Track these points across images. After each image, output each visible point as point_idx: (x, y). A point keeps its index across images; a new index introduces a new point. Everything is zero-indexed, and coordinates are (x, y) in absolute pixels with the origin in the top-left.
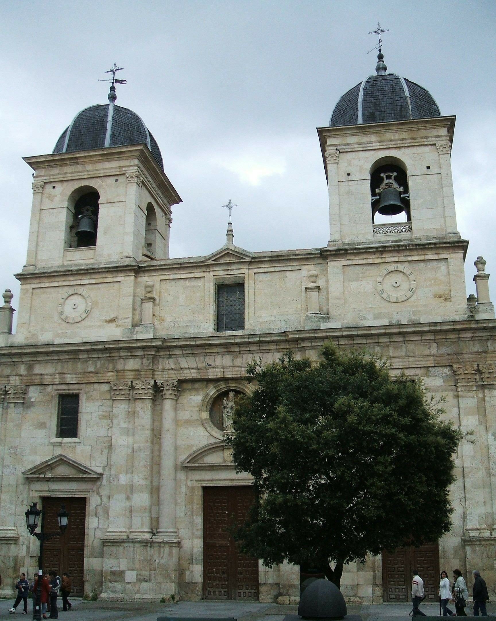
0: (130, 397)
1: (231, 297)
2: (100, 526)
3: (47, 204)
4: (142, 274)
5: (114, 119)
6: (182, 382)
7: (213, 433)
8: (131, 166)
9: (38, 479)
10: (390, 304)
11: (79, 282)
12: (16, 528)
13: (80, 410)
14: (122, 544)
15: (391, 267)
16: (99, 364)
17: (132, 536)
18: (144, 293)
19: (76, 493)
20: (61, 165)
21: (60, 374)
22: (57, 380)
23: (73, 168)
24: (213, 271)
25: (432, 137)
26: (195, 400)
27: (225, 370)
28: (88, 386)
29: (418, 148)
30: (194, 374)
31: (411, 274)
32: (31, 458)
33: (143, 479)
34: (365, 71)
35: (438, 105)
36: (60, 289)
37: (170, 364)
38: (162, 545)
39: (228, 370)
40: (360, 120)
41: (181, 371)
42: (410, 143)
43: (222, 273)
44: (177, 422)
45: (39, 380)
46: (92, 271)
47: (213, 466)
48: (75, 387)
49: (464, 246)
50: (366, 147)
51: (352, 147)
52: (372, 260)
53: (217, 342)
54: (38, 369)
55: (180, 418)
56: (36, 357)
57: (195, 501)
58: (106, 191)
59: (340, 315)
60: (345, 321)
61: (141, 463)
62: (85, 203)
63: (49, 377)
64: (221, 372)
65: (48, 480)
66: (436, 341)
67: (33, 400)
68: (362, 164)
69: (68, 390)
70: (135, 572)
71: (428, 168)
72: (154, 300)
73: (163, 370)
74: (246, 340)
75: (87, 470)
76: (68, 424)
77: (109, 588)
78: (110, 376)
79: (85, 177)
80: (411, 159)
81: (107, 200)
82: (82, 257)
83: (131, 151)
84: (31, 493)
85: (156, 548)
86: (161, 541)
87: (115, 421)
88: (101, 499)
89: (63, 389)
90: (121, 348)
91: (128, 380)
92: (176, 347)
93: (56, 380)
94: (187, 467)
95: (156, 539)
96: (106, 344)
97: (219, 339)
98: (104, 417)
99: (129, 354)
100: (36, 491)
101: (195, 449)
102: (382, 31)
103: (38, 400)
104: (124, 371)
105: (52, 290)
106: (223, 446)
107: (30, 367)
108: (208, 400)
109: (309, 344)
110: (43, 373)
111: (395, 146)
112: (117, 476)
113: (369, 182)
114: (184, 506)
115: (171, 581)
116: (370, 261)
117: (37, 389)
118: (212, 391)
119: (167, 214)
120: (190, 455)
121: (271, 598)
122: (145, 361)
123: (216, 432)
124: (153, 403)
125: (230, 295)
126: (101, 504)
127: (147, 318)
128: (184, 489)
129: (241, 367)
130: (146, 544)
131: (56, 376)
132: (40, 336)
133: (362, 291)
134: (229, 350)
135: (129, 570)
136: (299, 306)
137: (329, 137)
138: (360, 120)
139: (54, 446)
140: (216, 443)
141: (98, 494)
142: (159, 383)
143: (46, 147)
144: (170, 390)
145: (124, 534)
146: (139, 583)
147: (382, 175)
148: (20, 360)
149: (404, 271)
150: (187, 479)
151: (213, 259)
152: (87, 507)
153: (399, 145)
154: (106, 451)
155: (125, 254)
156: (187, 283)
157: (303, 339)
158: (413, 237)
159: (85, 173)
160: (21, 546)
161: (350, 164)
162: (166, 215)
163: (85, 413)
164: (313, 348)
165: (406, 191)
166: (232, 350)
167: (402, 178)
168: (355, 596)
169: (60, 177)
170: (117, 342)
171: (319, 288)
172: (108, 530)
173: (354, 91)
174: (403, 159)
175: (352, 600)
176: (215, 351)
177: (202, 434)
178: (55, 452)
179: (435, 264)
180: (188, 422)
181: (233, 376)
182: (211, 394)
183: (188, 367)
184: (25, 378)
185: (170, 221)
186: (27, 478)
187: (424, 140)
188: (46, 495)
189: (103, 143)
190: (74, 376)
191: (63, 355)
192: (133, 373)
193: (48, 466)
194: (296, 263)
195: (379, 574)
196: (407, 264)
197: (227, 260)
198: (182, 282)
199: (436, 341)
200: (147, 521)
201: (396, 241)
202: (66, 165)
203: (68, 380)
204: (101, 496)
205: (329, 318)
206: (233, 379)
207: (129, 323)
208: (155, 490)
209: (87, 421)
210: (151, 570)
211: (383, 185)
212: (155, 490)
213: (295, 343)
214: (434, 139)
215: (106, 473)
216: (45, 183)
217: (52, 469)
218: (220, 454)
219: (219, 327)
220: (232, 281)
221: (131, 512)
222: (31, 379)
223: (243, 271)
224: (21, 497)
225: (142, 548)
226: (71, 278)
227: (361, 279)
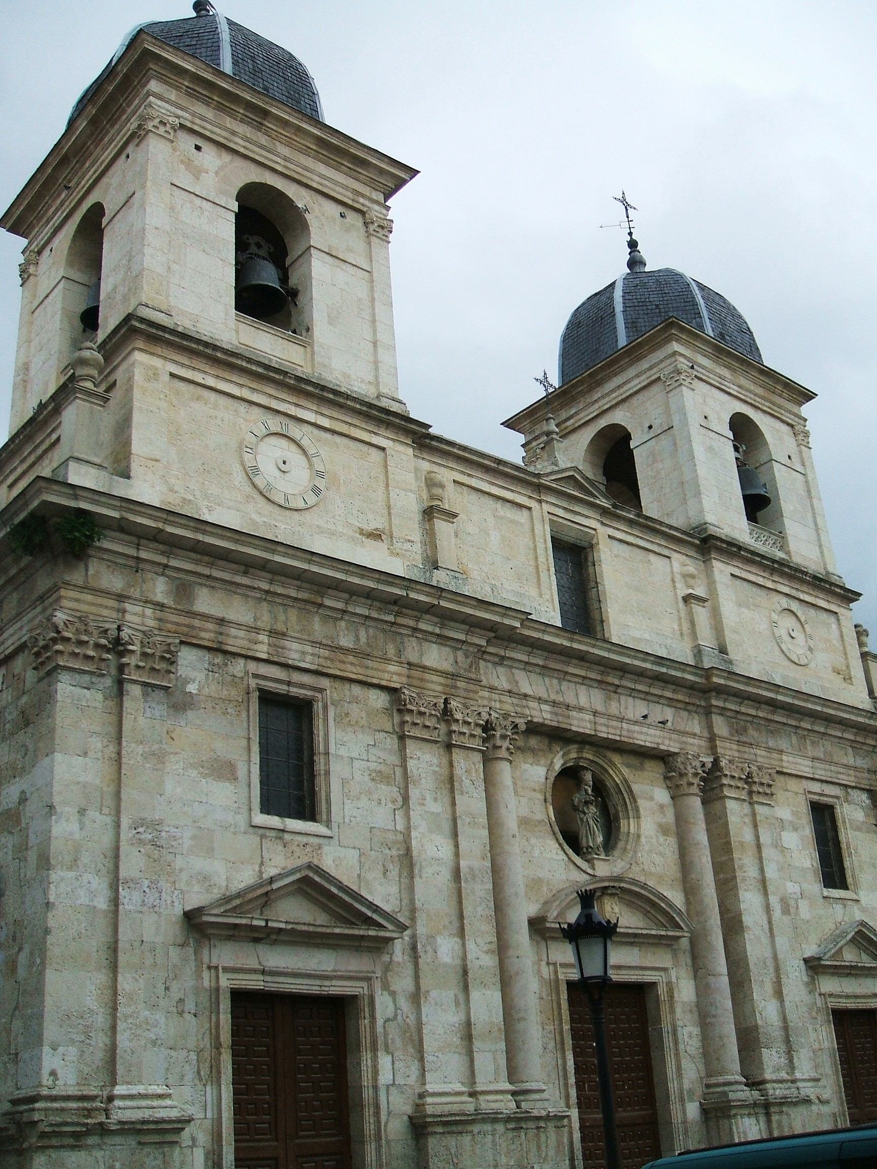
10: (790, 664)
14: (469, 1128)
19: (334, 983)
20: (220, 108)
21: (273, 633)
28: (338, 684)
33: (487, 953)
37: (499, 677)
43: (560, 512)
46: (331, 396)
48: (306, 679)
54: (206, 602)
56: (211, 565)
61: (479, 909)
63: (241, 634)
66: (854, 745)
67: (192, 688)
93: (259, 647)
96: (413, 589)
105: (223, 401)
107: (183, 591)
112: (431, 938)
117: (201, 659)
137: (677, 341)
139: (262, 837)
151: (554, 477)
154: (394, 871)
159: (279, 160)
169: (219, 135)
173: (612, 285)
177: (555, 857)
190: (309, 649)
191: (283, 584)
192: (442, 680)
193: (264, 895)
199: (854, 745)
202: (232, 114)
203: (295, 656)
209: (344, 782)
214: (796, 419)
222: (192, 627)
225: (510, 1135)
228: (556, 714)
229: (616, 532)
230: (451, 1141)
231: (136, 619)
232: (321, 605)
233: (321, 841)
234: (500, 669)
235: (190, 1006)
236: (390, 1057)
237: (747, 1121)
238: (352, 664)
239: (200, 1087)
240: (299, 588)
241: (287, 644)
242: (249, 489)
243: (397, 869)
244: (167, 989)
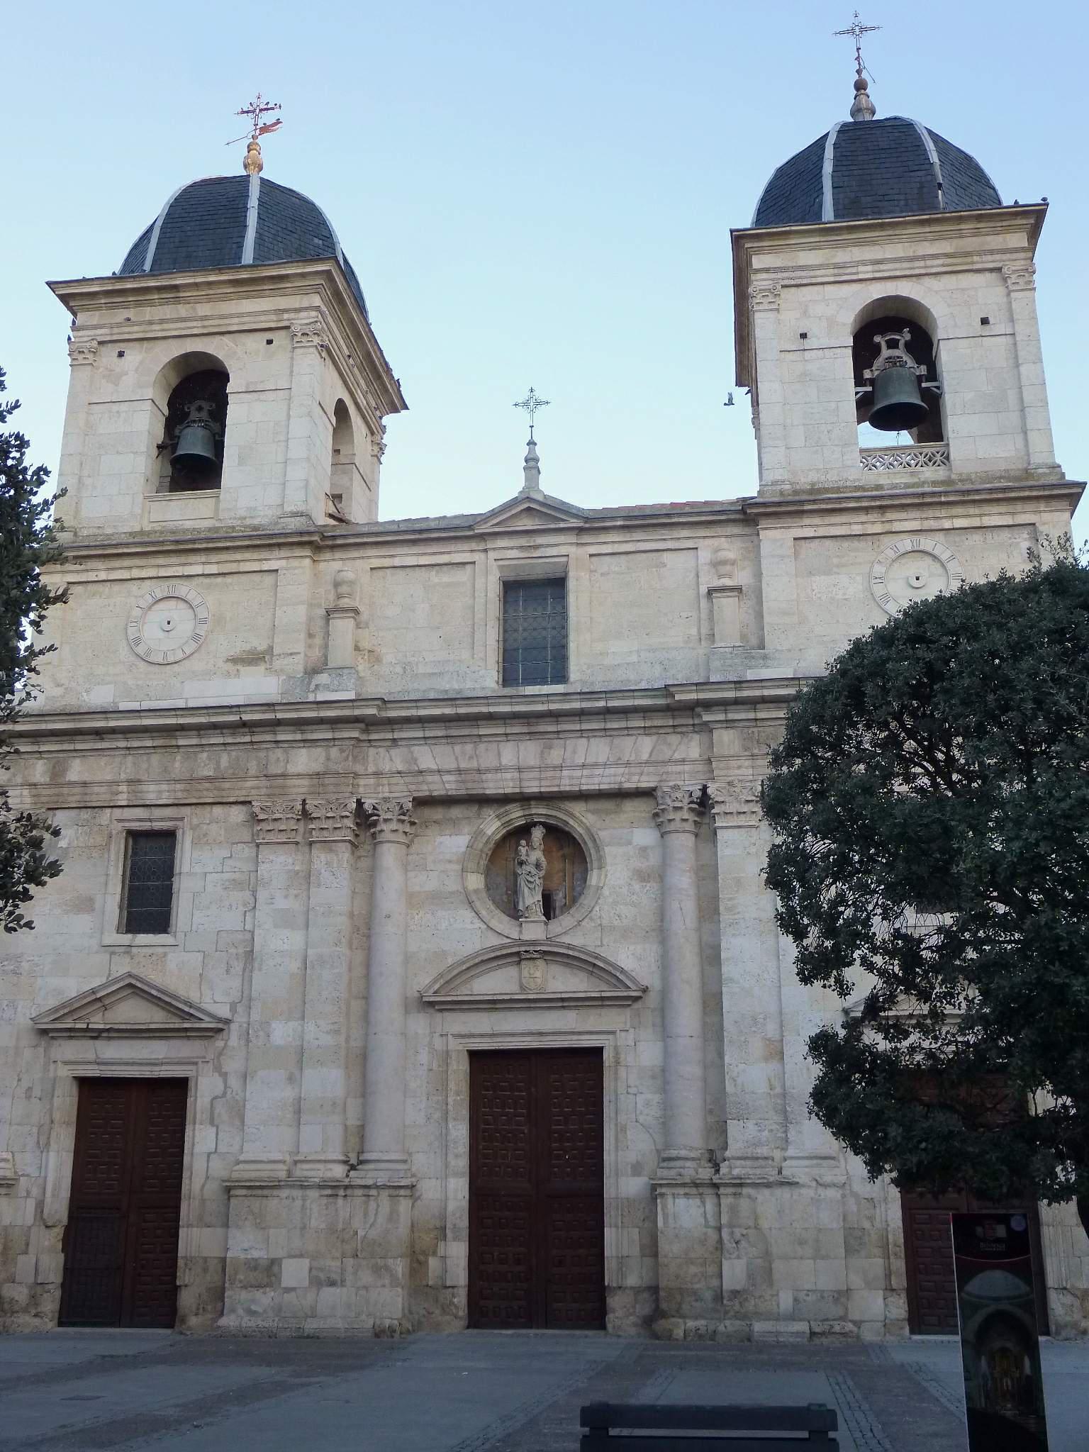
0: (299, 839)
1: (535, 610)
2: (222, 1149)
3: (106, 391)
4: (327, 555)
5: (261, 203)
6: (422, 802)
7: (494, 923)
8: (306, 309)
9: (72, 1034)
11: (179, 571)
12: (9, 1156)
13: (177, 870)
14: (275, 1192)
15: (906, 543)
16: (225, 760)
17: (300, 1171)
18: (332, 597)
19: (163, 1068)
22: (125, 796)
23: (168, 311)
24: (494, 549)
25: (992, 252)
26: (454, 844)
27: (525, 776)
28: (199, 810)
29: (960, 276)
30: (450, 785)
31: (952, 557)
33: (328, 1033)
34: (832, 114)
35: (997, 187)
36: (133, 587)
37: (393, 760)
38: (373, 1192)
39: (532, 775)
40: (828, 212)
41: (421, 779)
42: (943, 265)
44: (413, 900)
47: (494, 1002)
49: (1071, 495)
50: (840, 275)
51: (812, 273)
52: (860, 527)
53: (507, 709)
54: (76, 771)
55: (417, 888)
57: (452, 1085)
58: (245, 365)
59: (789, 650)
60: (802, 664)
62: (198, 392)
63: (103, 789)
64: (512, 779)
65: (96, 1035)
68: (835, 312)
69: (150, 820)
70: (306, 1263)
71: (985, 321)
72: (356, 611)
73: (377, 774)
74: (576, 705)
75: (192, 1011)
78: (249, 788)
79: (196, 331)
80: (946, 303)
81: (248, 385)
82: (190, 511)
83: (303, 275)
84: (52, 1067)
85: (359, 1201)
86: (370, 1182)
87: (262, 895)
88: (225, 1082)
89: (138, 819)
90: (279, 722)
91: (294, 797)
92: (408, 721)
93: (120, 797)
94: (431, 1004)
95: (357, 1178)
96: (245, 712)
97: (511, 704)
98: (236, 885)
99: (299, 737)
100: (66, 1063)
101: (450, 961)
102: (863, 30)
104: (284, 776)
106: (518, 953)
108: (481, 845)
109: (721, 717)
110: (88, 779)
111: (908, 272)
112: (265, 1024)
113: (850, 351)
114: (424, 1098)
115: (395, 1283)
116: (857, 529)
118: (492, 825)
119: (376, 431)
120: (441, 975)
121: (635, 1325)
122: (334, 752)
123: (501, 922)
124: (353, 853)
125: (535, 601)
126: (224, 1094)
127: (342, 651)
128: (424, 1057)
129: (561, 768)
130: (333, 1189)
131: (120, 788)
133: (840, 597)
134: (533, 729)
136: (694, 631)
137: (760, 251)
138: (828, 212)
140: (503, 947)
141: (218, 1068)
142: (367, 807)
143: (106, 260)
144: (395, 821)
145: (281, 1166)
147: (877, 339)
148: (35, 748)
149: (936, 552)
150: (432, 1033)
151: (495, 521)
152: (190, 1101)
153: (917, 272)
154: (238, 967)
155: (289, 508)
156: (434, 577)
157: (708, 705)
158: (953, 477)
161: (805, 313)
162: (372, 433)
163: (190, 874)
164: (729, 724)
165: (933, 374)
166: (541, 728)
167: (923, 346)
168: (843, 1318)
170: (270, 706)
171: (739, 589)
172: (242, 1158)
173: (820, 144)
174: (926, 302)
175: (837, 1329)
176: (500, 730)
178: (114, 968)
179: (1005, 534)
180: (437, 898)
181: (543, 790)
182: (489, 832)
183: (435, 767)
184: (44, 792)
185: (382, 449)
186: (44, 1032)
187: (976, 258)
188: (90, 1074)
189: (239, 257)
190: (164, 787)
193: (97, 1000)
194: (685, 533)
195: (899, 1265)
196: (940, 537)
197: (528, 523)
198: (422, 573)
200: (336, 1133)
201: (913, 485)
202: (151, 303)
203: (152, 796)
204: (226, 1074)
205: (765, 657)
206: (542, 798)
207: (296, 666)
208: (361, 1062)
210: (343, 1256)
211: (878, 363)
212: (361, 1062)
213: (689, 713)
214: (997, 257)
215: (240, 1019)
216: (100, 343)
217: (105, 1008)
218: (512, 971)
219: (508, 678)
220: (538, 573)
221: (298, 1112)
223: (563, 550)
225: (324, 1201)
226: (161, 560)
227: (835, 570)
228: (463, 782)
229: (604, 546)
230: (256, 1204)
231: (18, 801)
232: (178, 747)
233: (167, 949)
234: (394, 752)
235: (37, 1092)
236: (214, 1129)
237: (681, 1202)
238: (207, 790)
239: (38, 1153)
240: (152, 738)
241: (144, 788)
242: (133, 658)
243: (242, 965)
244: (19, 1080)
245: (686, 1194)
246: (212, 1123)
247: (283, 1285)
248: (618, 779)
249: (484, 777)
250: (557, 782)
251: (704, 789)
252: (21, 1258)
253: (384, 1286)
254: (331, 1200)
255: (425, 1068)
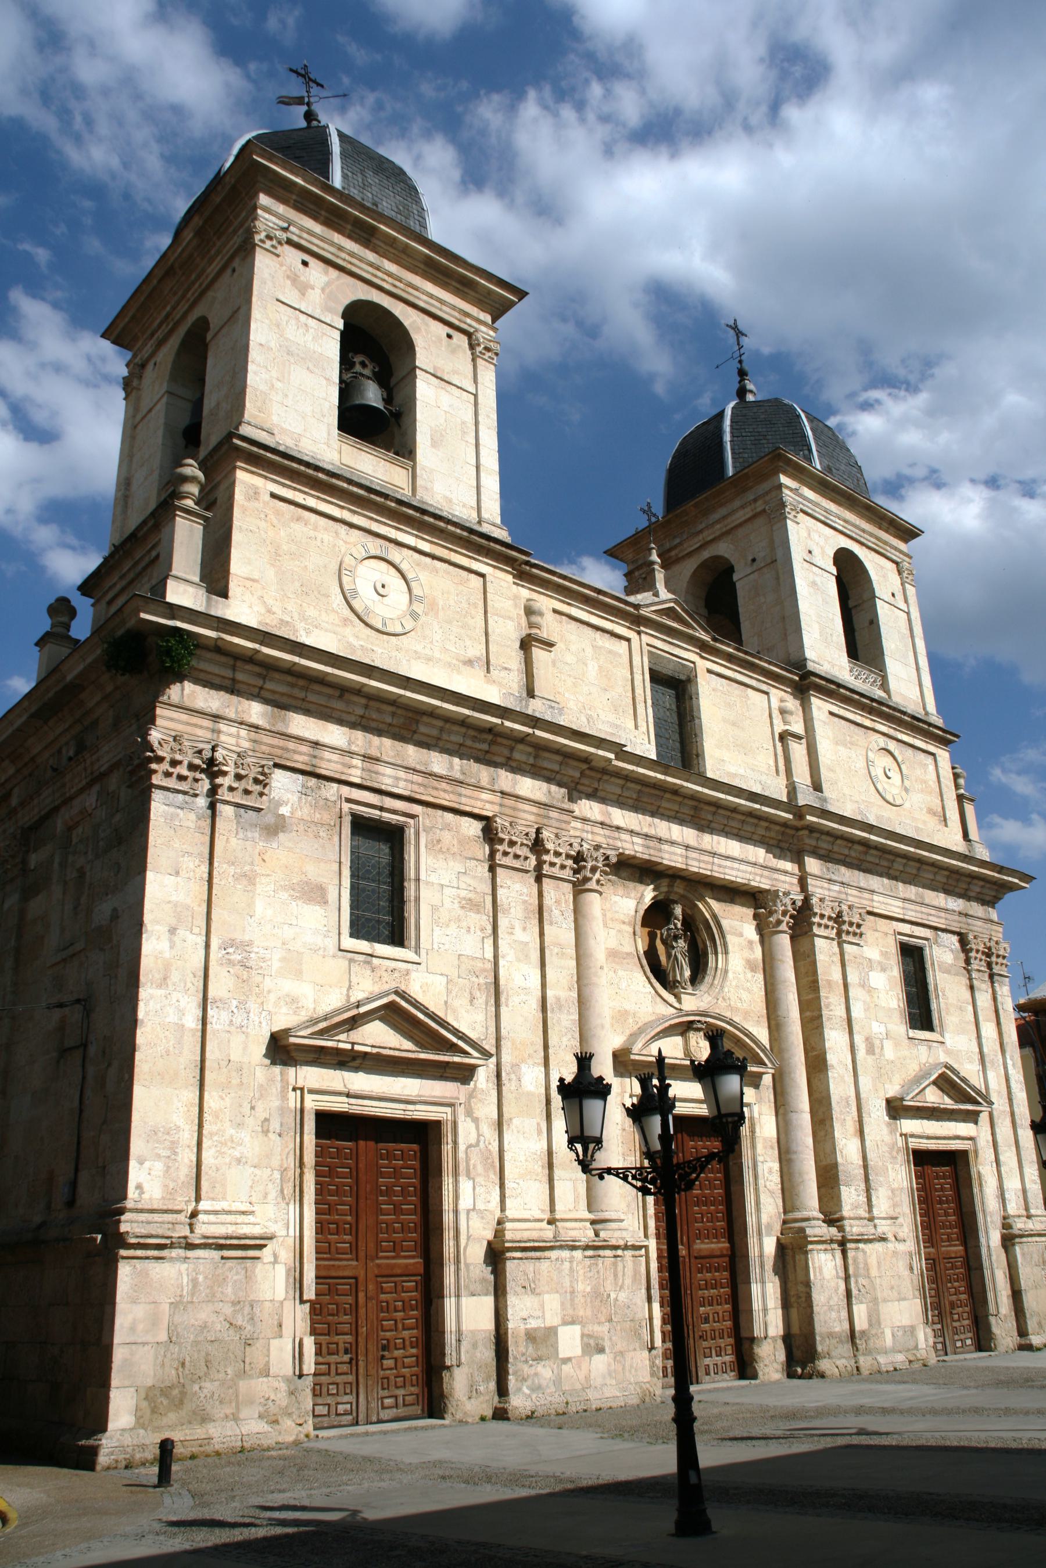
14: (547, 1254)
19: (418, 1107)
26: (630, 901)
32: (288, 986)
38: (619, 1252)
41: (616, 834)
45: (306, 758)
61: (565, 1039)
76: (382, 909)
77: (524, 1380)
88: (477, 1128)
93: (353, 771)
103: (299, 814)
126: (478, 1141)
132: (303, 633)
135: (565, 1323)
146: (587, 1358)
160: (270, 1267)
181: (701, 871)
190: (402, 774)
192: (535, 810)
209: (434, 909)
224: (260, 1106)
225: (588, 1262)
235: (275, 1125)
236: (471, 1182)
238: (445, 791)
239: (283, 1205)
243: (484, 997)
245: (826, 1250)
246: (469, 1178)
247: (561, 1356)
248: (748, 876)
249: (663, 847)
250: (709, 867)
251: (538, 831)
252: (275, 1343)
253: (635, 1350)
254: (593, 1261)
255: (619, 1127)
